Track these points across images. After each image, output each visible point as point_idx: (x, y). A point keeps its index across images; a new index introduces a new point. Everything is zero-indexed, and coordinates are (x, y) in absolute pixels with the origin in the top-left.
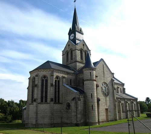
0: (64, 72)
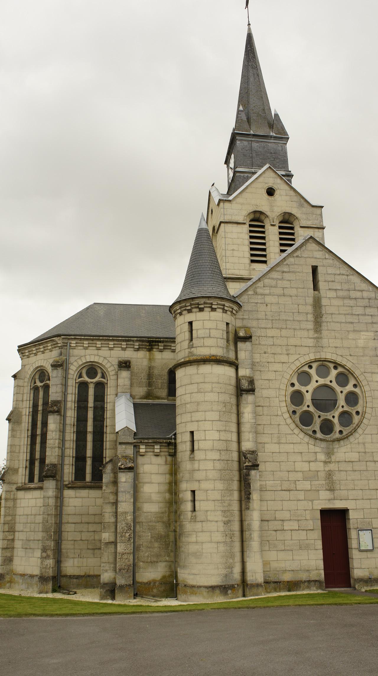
0: (123, 340)
